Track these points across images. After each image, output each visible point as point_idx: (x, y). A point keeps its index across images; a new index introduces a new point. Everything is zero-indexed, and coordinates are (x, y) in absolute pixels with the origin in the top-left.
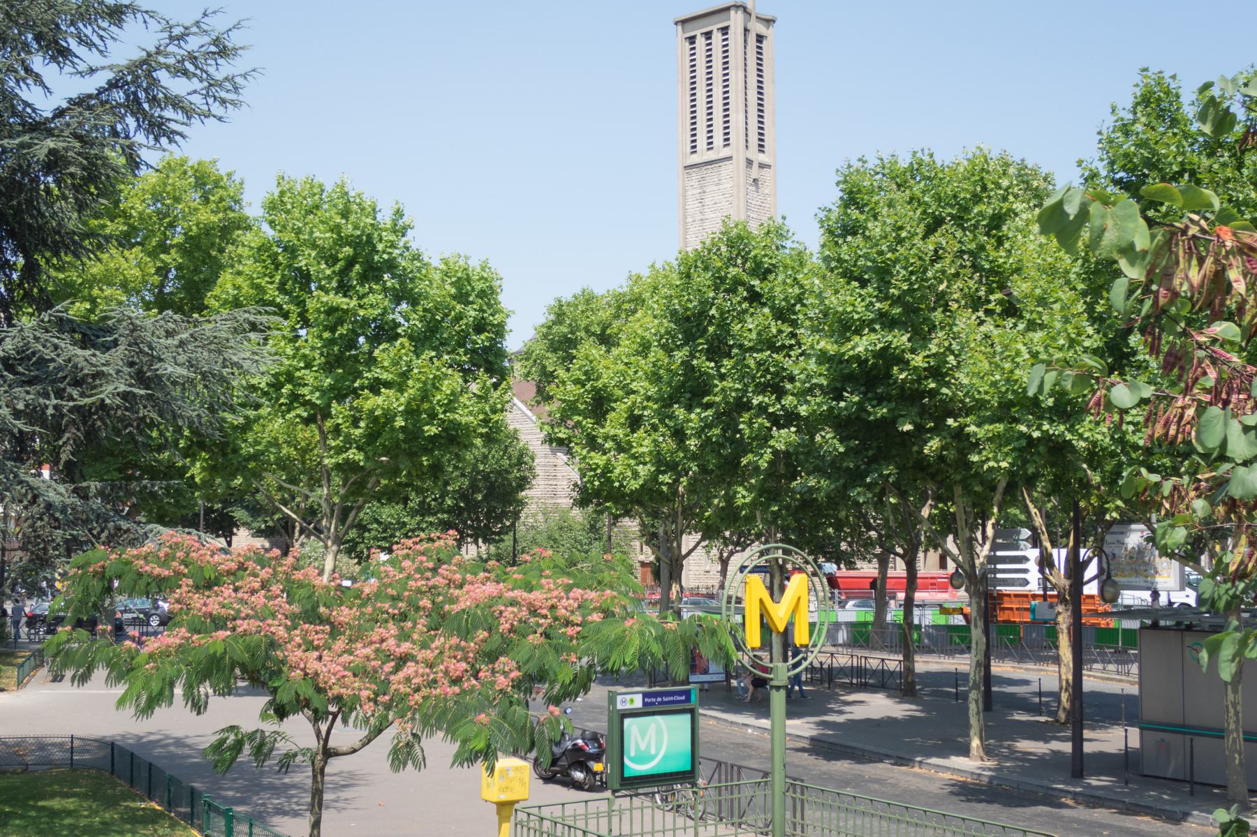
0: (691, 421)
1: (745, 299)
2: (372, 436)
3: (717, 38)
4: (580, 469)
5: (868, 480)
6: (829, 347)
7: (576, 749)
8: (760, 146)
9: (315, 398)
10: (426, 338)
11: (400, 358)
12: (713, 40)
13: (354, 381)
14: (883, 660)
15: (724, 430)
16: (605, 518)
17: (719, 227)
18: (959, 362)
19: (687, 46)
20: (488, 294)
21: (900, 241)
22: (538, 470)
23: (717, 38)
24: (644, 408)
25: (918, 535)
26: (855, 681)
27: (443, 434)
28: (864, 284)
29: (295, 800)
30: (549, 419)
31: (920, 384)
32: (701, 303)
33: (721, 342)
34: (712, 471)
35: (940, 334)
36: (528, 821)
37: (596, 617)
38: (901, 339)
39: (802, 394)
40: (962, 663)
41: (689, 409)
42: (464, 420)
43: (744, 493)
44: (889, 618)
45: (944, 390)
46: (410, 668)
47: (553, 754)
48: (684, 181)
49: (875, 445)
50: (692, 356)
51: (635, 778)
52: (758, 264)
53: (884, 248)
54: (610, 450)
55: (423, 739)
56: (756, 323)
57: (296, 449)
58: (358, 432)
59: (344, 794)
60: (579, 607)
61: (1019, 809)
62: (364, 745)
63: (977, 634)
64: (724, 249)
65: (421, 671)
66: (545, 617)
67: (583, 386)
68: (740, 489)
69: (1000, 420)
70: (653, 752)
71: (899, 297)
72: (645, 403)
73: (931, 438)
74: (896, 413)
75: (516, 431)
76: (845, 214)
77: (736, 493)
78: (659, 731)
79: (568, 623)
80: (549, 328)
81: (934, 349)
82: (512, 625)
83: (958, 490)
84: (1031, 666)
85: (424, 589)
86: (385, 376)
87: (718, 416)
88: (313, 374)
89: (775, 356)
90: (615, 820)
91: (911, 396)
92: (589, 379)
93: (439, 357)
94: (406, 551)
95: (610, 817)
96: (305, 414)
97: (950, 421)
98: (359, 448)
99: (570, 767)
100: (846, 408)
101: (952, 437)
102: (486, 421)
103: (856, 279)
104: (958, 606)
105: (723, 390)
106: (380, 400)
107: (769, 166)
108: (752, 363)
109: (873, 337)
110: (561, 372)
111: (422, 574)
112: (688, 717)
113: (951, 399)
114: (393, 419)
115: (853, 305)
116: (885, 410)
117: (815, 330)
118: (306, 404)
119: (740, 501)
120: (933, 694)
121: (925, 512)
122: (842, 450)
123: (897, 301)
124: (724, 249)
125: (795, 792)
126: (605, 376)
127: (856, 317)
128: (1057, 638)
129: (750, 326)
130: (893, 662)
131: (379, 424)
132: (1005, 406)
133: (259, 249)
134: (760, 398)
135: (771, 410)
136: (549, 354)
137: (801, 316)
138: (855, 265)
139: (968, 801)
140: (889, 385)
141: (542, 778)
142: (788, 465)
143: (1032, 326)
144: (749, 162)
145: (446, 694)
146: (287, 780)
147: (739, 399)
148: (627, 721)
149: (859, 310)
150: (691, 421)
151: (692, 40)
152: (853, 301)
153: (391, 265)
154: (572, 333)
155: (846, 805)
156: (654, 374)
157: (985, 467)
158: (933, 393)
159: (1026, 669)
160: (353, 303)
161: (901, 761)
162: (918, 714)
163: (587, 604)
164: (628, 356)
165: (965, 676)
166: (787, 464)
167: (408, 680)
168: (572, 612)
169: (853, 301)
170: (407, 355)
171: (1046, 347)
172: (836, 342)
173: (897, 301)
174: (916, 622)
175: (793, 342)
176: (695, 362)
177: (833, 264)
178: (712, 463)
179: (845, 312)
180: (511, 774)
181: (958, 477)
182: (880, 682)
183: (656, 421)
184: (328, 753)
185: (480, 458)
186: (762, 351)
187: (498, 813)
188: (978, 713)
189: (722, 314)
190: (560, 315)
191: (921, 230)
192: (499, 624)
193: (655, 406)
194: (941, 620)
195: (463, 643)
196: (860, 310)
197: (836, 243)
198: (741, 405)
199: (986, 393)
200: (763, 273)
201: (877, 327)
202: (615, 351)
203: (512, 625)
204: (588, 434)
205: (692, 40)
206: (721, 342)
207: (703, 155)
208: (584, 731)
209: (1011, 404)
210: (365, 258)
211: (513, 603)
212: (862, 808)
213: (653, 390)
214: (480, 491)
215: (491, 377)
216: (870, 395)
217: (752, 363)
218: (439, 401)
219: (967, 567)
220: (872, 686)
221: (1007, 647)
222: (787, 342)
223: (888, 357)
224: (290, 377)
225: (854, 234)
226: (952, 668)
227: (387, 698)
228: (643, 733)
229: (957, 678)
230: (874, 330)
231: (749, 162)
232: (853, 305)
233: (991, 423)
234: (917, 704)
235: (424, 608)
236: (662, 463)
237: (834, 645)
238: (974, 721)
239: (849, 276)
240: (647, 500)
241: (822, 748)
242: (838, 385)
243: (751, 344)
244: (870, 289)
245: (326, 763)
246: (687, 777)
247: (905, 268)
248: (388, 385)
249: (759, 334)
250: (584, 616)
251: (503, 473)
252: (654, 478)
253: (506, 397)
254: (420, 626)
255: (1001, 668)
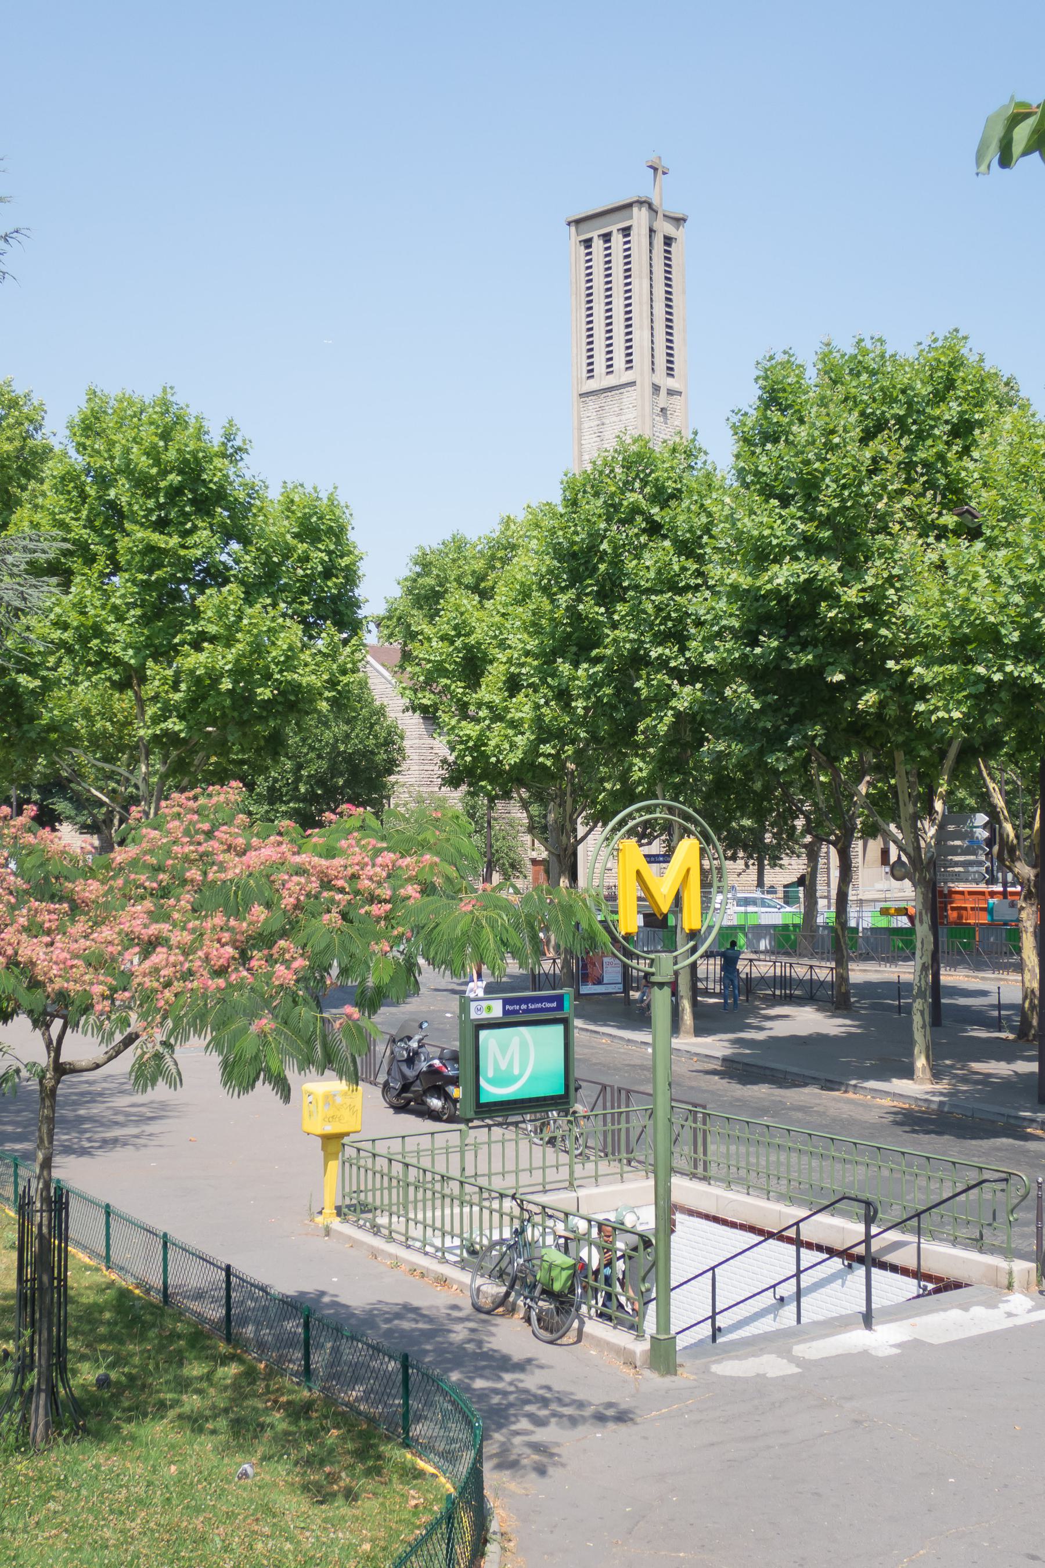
0: (578, 679)
1: (644, 531)
2: (193, 702)
3: (617, 239)
4: (449, 742)
5: (790, 743)
6: (741, 580)
7: (433, 1071)
8: (669, 368)
9: (129, 656)
10: (264, 583)
11: (227, 607)
12: (613, 243)
13: (174, 637)
14: (811, 967)
15: (618, 691)
16: (483, 801)
17: (611, 444)
18: (900, 598)
19: (583, 251)
20: (338, 533)
21: (832, 448)
22: (408, 752)
23: (617, 239)
24: (522, 665)
25: (853, 818)
26: (778, 992)
27: (280, 699)
28: (785, 501)
29: (88, 1135)
30: (410, 684)
31: (853, 624)
32: (590, 535)
33: (614, 584)
34: (604, 738)
35: (878, 563)
36: (358, 1158)
37: (411, 890)
38: (829, 569)
39: (708, 641)
40: (905, 972)
41: (576, 665)
42: (304, 681)
43: (641, 764)
44: (820, 920)
45: (883, 631)
46: (160, 956)
47: (404, 1076)
48: (579, 412)
49: (798, 700)
50: (579, 599)
51: (495, 1104)
52: (660, 489)
53: (811, 456)
54: (484, 719)
55: (177, 1048)
56: (656, 558)
57: (113, 723)
58: (177, 696)
59: (149, 1128)
60: (389, 876)
61: (974, 1142)
62: (110, 1059)
63: (923, 931)
64: (618, 470)
65: (172, 959)
66: (342, 890)
67: (452, 643)
68: (636, 760)
69: (953, 661)
70: (516, 1072)
71: (828, 518)
72: (523, 659)
73: (866, 691)
74: (824, 660)
75: (383, 707)
76: (766, 418)
77: (632, 765)
78: (524, 1045)
79: (373, 899)
80: (415, 581)
81: (870, 581)
82: (298, 899)
83: (900, 756)
84: (989, 975)
85: (194, 856)
86: (212, 629)
87: (609, 672)
88: (125, 628)
89: (677, 598)
90: (469, 1156)
91: (842, 640)
92: (459, 635)
93: (274, 605)
94: (176, 809)
95: (462, 1153)
96: (116, 677)
97: (890, 664)
98: (182, 717)
99: (426, 1092)
100: (762, 656)
101: (892, 689)
102: (332, 683)
103: (776, 497)
104: (903, 905)
105: (614, 640)
106: (202, 657)
107: (679, 393)
108: (649, 608)
109: (796, 566)
110: (428, 630)
111: (192, 837)
112: (560, 1029)
113: (891, 643)
114: (216, 680)
115: (772, 528)
116: (810, 657)
117: (725, 562)
118: (117, 662)
119: (636, 775)
120: (873, 1007)
121: (863, 788)
122: (757, 706)
123: (825, 522)
124: (618, 470)
125: (695, 1121)
126: (478, 631)
127: (775, 542)
128: (1020, 938)
129: (648, 564)
130: (824, 972)
131: (204, 686)
132: (959, 642)
133: (63, 478)
134: (660, 650)
135: (673, 664)
136: (415, 612)
137: (708, 550)
138: (776, 479)
139: (914, 1131)
140: (816, 626)
141: (392, 1107)
142: (696, 731)
143: (992, 544)
144: (656, 388)
145: (206, 988)
146: (82, 1112)
147: (634, 652)
148: (483, 1034)
149: (779, 534)
150: (578, 679)
151: (588, 243)
152: (774, 523)
153: (220, 496)
154: (441, 585)
155: (757, 1137)
156: (534, 624)
157: (934, 718)
158: (869, 636)
159: (983, 979)
160: (175, 540)
161: (829, 1085)
162: (853, 1030)
163: (399, 872)
164: (505, 605)
165: (909, 986)
166: (691, 728)
167: (156, 970)
168: (379, 883)
169: (774, 523)
170: (235, 603)
171: (1011, 571)
172: (750, 574)
173: (825, 522)
174: (852, 924)
175: (699, 581)
176: (581, 607)
177: (749, 479)
178: (604, 730)
179: (762, 537)
180: (339, 1100)
181: (900, 739)
182: (809, 994)
183: (536, 680)
184: (61, 1070)
185: (340, 736)
186: (662, 592)
187: (324, 1148)
188: (924, 1027)
189: (615, 548)
190: (425, 565)
191: (857, 433)
192: (281, 898)
193: (536, 663)
194: (882, 922)
195: (232, 922)
196: (780, 534)
197: (753, 453)
198: (637, 660)
199: (935, 627)
200: (663, 497)
201: (801, 554)
202: (488, 604)
203: (298, 899)
204: (459, 700)
205: (588, 243)
206: (614, 584)
207: (601, 381)
208: (443, 1049)
209: (966, 640)
210: (194, 489)
211: (301, 871)
212: (777, 1141)
213: (532, 644)
214: (341, 775)
215: (340, 632)
216: (791, 639)
217: (649, 608)
218: (275, 658)
219: (910, 850)
220: (798, 997)
221: (959, 953)
222: (692, 582)
223: (814, 592)
224: (97, 631)
225: (776, 441)
226: (894, 978)
227: (127, 994)
228: (504, 1048)
229: (899, 989)
230: (797, 559)
231: (656, 388)
232: (772, 528)
233: (941, 665)
234: (852, 1019)
235: (192, 881)
236: (545, 733)
237: (756, 952)
238: (918, 1036)
239: (767, 493)
240: (528, 776)
241: (736, 1069)
242: (754, 628)
243: (649, 585)
244: (792, 509)
245: (58, 1082)
246: (561, 1102)
247: (836, 481)
248: (213, 639)
249: (659, 572)
250: (394, 889)
251: (368, 754)
252: (533, 750)
253: (358, 656)
254: (182, 903)
255: (951, 977)
